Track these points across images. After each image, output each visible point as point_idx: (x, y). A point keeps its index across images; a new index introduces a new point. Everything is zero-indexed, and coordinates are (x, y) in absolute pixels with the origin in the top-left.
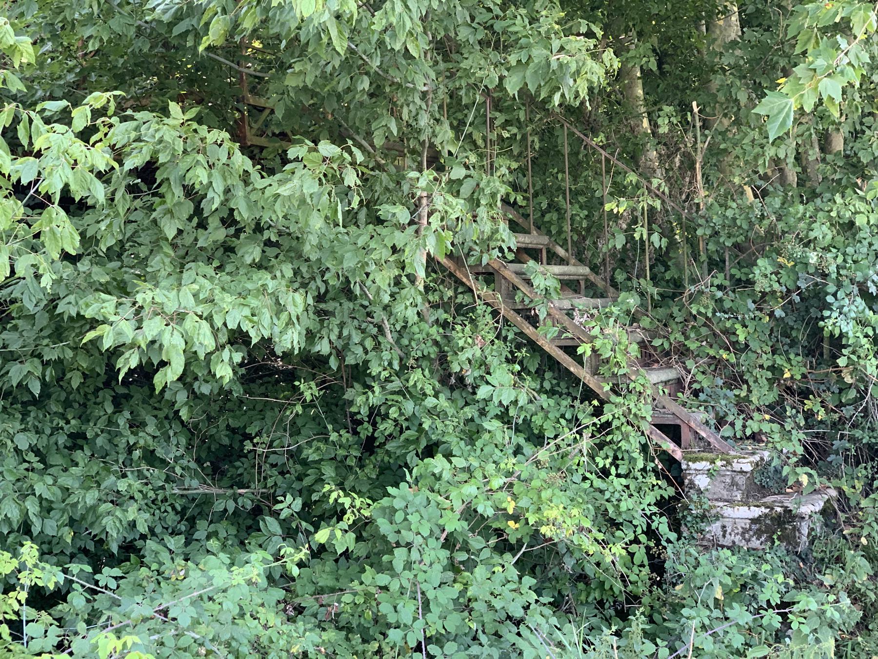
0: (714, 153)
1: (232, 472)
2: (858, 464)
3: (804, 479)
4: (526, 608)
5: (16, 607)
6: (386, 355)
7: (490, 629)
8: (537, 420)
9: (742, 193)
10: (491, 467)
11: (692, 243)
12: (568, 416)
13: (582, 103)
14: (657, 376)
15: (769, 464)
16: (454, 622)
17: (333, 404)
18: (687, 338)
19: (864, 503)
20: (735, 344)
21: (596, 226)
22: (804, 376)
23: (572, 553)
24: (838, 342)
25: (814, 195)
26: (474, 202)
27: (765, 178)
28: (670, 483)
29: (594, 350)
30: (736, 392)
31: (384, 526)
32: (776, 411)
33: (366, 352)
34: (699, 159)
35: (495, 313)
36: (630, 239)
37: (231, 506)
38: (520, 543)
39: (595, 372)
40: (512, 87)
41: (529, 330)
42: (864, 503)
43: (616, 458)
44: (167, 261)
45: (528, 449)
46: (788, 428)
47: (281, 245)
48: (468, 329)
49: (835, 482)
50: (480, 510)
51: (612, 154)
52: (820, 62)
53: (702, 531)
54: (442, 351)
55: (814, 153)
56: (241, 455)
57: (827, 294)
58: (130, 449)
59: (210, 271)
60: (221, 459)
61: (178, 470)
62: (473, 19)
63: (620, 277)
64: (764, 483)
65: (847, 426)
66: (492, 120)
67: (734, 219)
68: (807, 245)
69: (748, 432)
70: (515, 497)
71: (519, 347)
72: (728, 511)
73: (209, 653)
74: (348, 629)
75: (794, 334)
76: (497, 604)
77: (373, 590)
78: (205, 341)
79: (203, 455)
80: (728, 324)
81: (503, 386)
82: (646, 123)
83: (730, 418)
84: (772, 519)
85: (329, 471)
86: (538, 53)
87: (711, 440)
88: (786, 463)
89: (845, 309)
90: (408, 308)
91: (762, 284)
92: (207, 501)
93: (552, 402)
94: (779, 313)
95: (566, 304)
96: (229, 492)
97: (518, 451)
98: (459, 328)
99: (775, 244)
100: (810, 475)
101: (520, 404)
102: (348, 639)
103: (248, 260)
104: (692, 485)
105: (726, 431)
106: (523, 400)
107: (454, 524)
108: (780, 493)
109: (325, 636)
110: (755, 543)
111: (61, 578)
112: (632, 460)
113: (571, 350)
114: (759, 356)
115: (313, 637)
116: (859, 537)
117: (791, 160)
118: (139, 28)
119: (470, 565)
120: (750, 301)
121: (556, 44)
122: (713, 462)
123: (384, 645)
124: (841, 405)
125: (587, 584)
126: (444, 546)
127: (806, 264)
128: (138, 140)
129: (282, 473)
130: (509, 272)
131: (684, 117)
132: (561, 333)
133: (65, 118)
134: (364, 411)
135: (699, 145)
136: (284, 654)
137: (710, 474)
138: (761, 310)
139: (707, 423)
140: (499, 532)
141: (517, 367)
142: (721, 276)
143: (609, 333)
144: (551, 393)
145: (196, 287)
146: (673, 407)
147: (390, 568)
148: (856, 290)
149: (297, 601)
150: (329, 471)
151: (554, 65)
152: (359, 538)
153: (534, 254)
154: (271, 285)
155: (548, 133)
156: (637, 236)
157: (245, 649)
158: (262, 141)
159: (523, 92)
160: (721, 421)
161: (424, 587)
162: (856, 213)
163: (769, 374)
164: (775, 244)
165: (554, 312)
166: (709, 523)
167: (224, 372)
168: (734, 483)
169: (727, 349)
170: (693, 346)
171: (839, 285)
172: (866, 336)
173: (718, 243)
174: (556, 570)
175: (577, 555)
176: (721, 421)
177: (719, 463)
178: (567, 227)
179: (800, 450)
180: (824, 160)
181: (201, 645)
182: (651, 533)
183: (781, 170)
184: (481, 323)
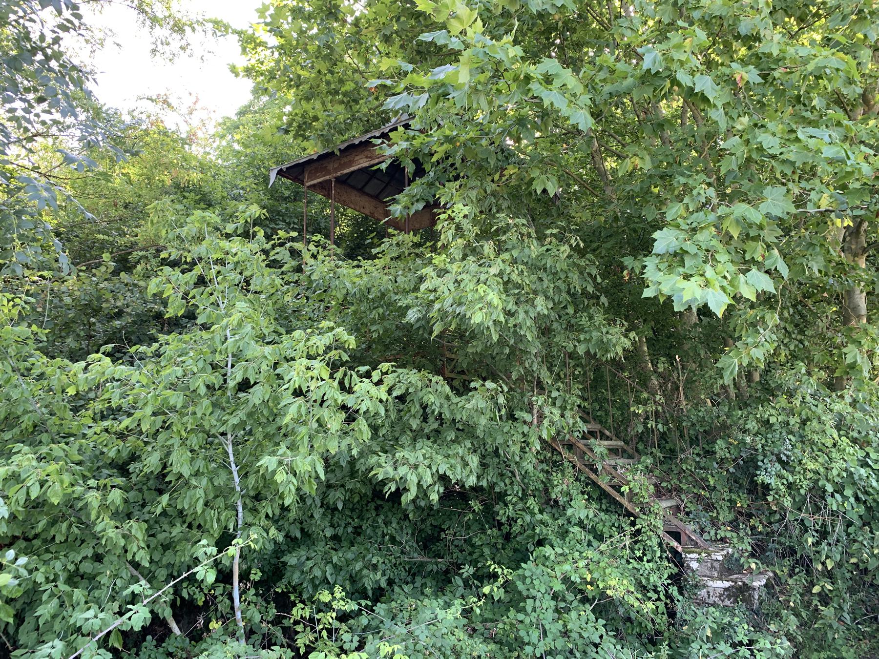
0: (689, 382)
1: (434, 548)
2: (784, 557)
3: (753, 566)
4: (601, 637)
5: (331, 621)
6: (516, 488)
7: (580, 648)
8: (599, 527)
9: (706, 402)
10: (577, 554)
11: (680, 429)
12: (616, 525)
13: (620, 358)
14: (665, 504)
15: (732, 555)
16: (560, 643)
17: (489, 512)
18: (681, 482)
19: (790, 581)
20: (708, 486)
21: (627, 419)
22: (748, 506)
23: (623, 606)
24: (767, 488)
25: (746, 405)
26: (563, 408)
27: (718, 395)
28: (676, 566)
29: (630, 489)
30: (711, 514)
31: (520, 586)
32: (734, 525)
33: (506, 485)
34: (681, 385)
35: (574, 467)
36: (646, 427)
37: (435, 568)
38: (594, 598)
39: (630, 501)
40: (581, 350)
41: (593, 476)
42: (790, 581)
43: (644, 549)
44: (409, 438)
45: (595, 543)
46: (741, 535)
47: (466, 430)
48: (559, 475)
49: (771, 567)
50: (572, 579)
51: (633, 381)
52: (750, 340)
53: (696, 594)
54: (545, 486)
55: (744, 383)
56: (438, 539)
57: (758, 461)
58: (384, 535)
59: (429, 443)
60: (429, 541)
61: (407, 547)
62: (560, 317)
63: (641, 447)
64: (730, 567)
65: (776, 535)
66: (569, 364)
67: (704, 417)
68: (744, 432)
69: (719, 537)
70: (591, 572)
71: (587, 485)
72: (710, 583)
73: (431, 653)
74: (499, 643)
75: (741, 481)
76: (585, 635)
77: (514, 622)
78: (428, 479)
79: (419, 539)
80: (704, 475)
81: (581, 509)
82: (650, 365)
83: (707, 529)
84: (736, 589)
85: (487, 551)
86: (595, 334)
87: (698, 541)
88: (742, 556)
89: (769, 470)
90: (529, 465)
91: (720, 454)
92: (422, 565)
93: (607, 516)
94: (732, 470)
95: (613, 463)
96: (434, 560)
97: (589, 544)
98: (554, 474)
99: (727, 431)
100: (756, 564)
101: (590, 517)
102: (501, 649)
103: (449, 439)
104: (689, 567)
105: (706, 536)
106: (591, 516)
107: (558, 587)
108: (739, 573)
109: (490, 647)
110: (727, 603)
111: (356, 607)
112: (654, 552)
113: (617, 488)
114: (722, 494)
115: (482, 647)
116: (789, 602)
117: (732, 386)
118: (397, 326)
119: (568, 610)
120: (715, 463)
121: (604, 330)
122: (700, 554)
123: (521, 654)
124: (770, 523)
125: (632, 623)
126: (553, 599)
127: (745, 443)
128: (399, 382)
129: (461, 551)
130: (581, 444)
131: (672, 364)
132: (611, 480)
133: (368, 375)
134: (504, 520)
135: (681, 378)
136: (469, 657)
137: (698, 560)
138: (722, 468)
139: (695, 531)
140: (581, 591)
141: (586, 497)
142: (698, 448)
143: (637, 480)
144: (607, 511)
145: (424, 451)
146: (675, 522)
147: (523, 610)
148: (775, 458)
149: (473, 625)
150: (487, 551)
151: (605, 340)
152: (506, 592)
153: (592, 434)
154: (461, 451)
155: (597, 370)
156: (649, 426)
157: (449, 652)
158: (453, 375)
159: (588, 353)
160: (702, 531)
161: (544, 622)
162: (771, 415)
163: (729, 504)
164: (727, 431)
165: (606, 467)
166: (700, 590)
167: (434, 497)
168: (713, 567)
169: (704, 489)
170: (685, 487)
171: (765, 456)
172: (783, 484)
173: (695, 430)
174: (614, 615)
175: (626, 606)
176: (702, 531)
177: (703, 555)
178: (610, 421)
179: (749, 549)
180: (749, 386)
181: (427, 649)
182: (668, 596)
183: (727, 392)
184: (567, 471)
